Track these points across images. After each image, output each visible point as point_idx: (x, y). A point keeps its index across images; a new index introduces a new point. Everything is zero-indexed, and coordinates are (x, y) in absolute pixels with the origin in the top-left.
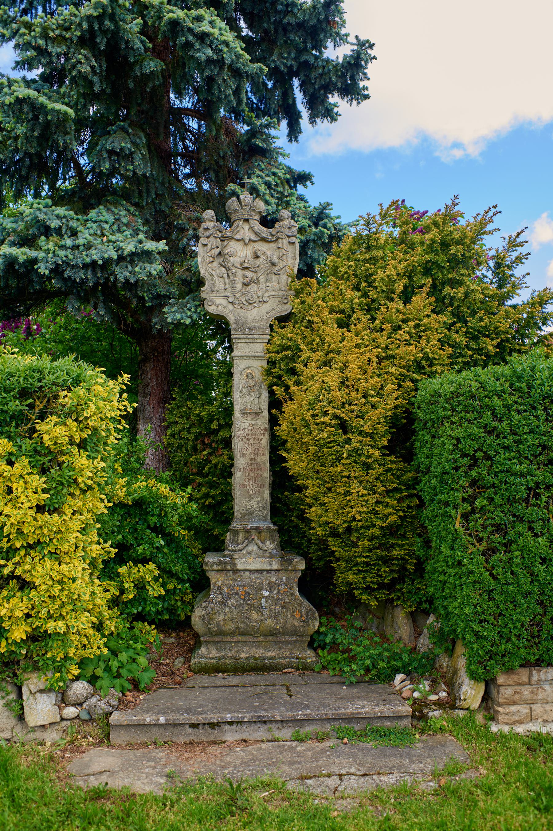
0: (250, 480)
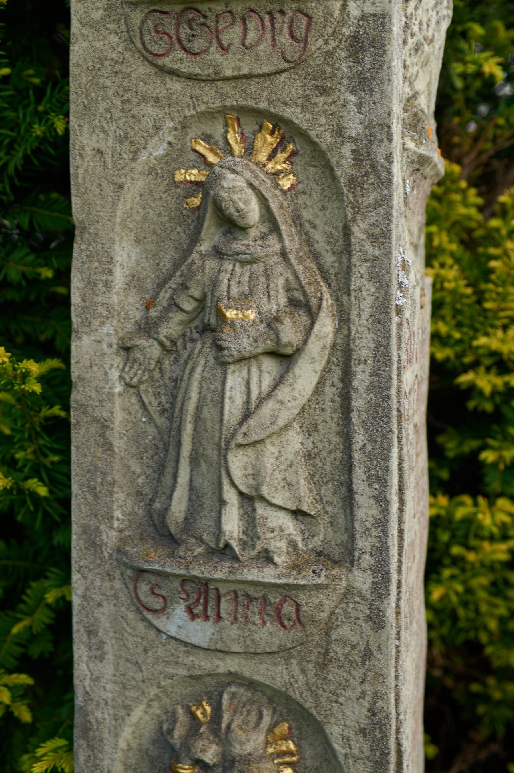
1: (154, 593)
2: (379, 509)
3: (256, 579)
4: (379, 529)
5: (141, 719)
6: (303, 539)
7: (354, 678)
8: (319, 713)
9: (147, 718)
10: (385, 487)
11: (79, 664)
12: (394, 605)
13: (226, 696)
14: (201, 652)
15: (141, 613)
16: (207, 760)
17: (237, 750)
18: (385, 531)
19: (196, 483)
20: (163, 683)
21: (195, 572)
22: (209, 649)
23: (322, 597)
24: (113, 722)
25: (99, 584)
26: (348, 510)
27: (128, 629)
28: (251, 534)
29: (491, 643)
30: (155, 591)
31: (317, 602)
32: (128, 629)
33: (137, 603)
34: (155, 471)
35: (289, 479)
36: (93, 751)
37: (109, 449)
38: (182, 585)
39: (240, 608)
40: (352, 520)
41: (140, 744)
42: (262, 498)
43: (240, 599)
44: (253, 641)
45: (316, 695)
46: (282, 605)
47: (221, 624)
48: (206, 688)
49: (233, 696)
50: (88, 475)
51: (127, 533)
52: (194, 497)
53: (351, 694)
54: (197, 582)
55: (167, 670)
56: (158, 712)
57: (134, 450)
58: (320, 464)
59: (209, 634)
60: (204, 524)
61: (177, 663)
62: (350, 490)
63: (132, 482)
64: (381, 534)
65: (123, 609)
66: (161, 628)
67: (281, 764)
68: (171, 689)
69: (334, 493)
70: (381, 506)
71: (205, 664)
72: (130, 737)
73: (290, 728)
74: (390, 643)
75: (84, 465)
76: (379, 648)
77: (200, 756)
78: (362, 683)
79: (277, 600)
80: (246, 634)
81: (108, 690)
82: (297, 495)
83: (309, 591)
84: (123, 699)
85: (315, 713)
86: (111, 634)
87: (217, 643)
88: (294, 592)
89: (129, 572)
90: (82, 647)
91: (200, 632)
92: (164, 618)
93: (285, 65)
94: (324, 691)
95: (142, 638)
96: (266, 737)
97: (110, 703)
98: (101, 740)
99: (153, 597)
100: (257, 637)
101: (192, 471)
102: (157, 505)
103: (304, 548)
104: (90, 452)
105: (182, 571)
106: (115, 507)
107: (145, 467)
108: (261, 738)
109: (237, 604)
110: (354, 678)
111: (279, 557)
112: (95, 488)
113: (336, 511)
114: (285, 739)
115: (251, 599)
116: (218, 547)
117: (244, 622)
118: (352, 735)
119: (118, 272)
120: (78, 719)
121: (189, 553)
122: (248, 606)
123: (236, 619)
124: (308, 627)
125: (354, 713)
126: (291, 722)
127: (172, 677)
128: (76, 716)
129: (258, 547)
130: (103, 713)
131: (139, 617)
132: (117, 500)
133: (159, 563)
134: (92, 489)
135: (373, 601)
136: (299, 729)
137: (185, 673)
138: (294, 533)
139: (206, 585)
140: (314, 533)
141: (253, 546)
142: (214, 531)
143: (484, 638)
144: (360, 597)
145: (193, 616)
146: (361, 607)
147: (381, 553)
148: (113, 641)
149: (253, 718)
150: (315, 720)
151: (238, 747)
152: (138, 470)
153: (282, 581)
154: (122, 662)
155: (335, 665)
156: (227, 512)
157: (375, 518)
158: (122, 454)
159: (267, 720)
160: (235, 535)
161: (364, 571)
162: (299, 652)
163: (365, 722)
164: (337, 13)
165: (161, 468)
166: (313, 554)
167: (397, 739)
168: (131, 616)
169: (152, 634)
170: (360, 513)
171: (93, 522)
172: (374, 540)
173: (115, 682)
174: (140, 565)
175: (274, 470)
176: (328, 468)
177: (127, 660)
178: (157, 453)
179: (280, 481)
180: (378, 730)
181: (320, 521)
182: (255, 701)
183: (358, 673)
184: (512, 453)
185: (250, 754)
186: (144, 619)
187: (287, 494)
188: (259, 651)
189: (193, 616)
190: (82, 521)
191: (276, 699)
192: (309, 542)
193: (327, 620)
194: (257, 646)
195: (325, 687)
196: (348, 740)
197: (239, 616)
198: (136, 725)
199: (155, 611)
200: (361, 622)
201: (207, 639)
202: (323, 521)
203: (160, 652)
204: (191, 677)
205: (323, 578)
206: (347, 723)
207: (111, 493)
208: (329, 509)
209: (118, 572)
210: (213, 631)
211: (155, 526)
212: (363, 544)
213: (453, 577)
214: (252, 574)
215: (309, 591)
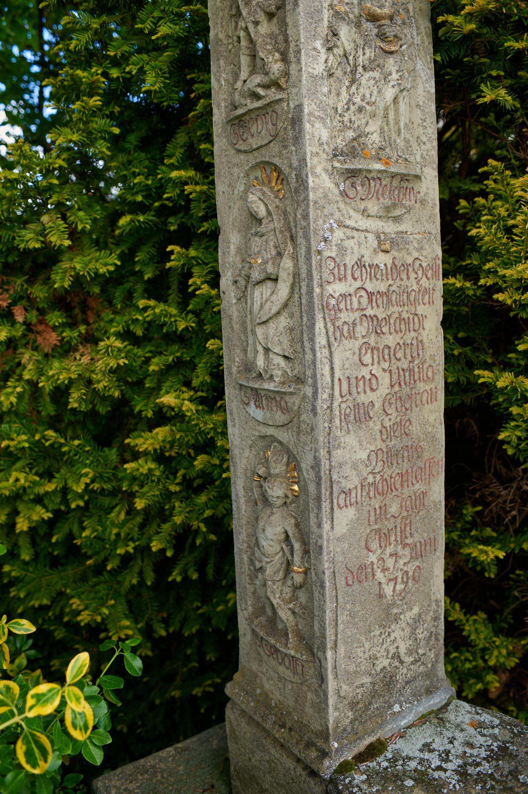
0: (384, 537)
93: (271, 138)
119: (232, 247)
149: (280, 458)
153: (276, 389)
164: (286, 108)
168: (241, 407)
183: (309, 437)
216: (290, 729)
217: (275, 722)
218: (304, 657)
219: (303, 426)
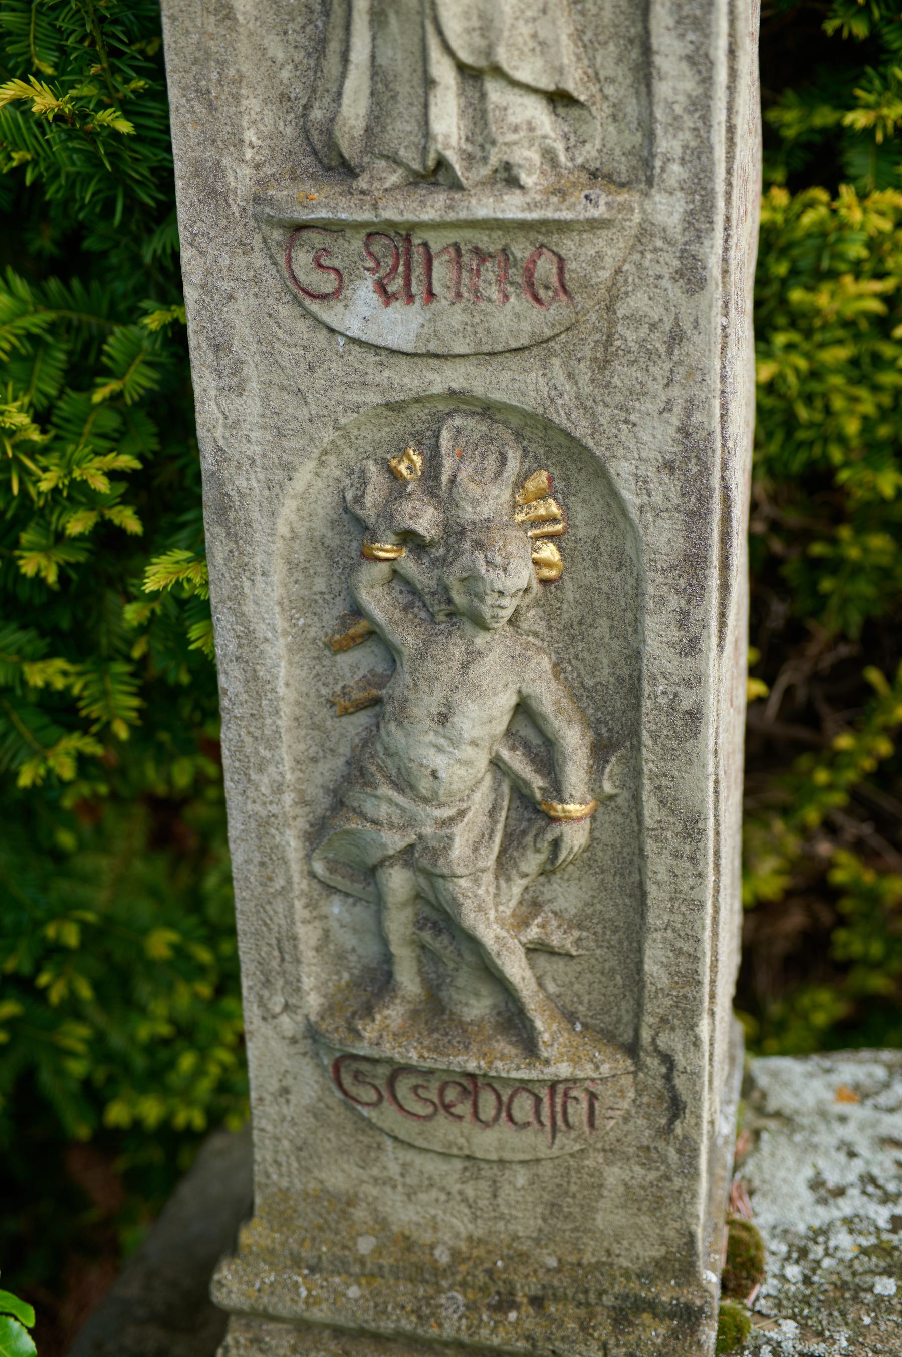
1: (320, 266)
2: (697, 78)
3: (491, 215)
4: (697, 115)
5: (310, 486)
6: (568, 149)
7: (655, 379)
8: (597, 444)
9: (320, 484)
10: (707, 36)
11: (203, 403)
12: (720, 251)
13: (445, 434)
14: (404, 361)
15: (300, 305)
16: (421, 531)
17: (467, 513)
18: (706, 119)
19: (381, 60)
20: (343, 421)
21: (389, 214)
22: (415, 355)
23: (602, 243)
24: (266, 493)
25: (227, 262)
26: (643, 89)
27: (280, 334)
28: (480, 139)
29: (847, 464)
30: (322, 262)
31: (593, 252)
32: (280, 334)
33: (292, 287)
34: (309, 55)
35: (542, 34)
36: (236, 542)
37: (227, 17)
38: (367, 246)
39: (465, 274)
40: (651, 104)
41: (310, 529)
42: (497, 71)
43: (465, 259)
44: (488, 331)
45: (593, 414)
46: (535, 262)
47: (434, 306)
48: (413, 426)
49: (458, 432)
50: (194, 68)
51: (268, 170)
52: (380, 86)
53: (650, 406)
54: (393, 234)
55: (348, 397)
56: (337, 473)
57: (270, 17)
58: (594, 10)
59: (414, 326)
60: (401, 132)
61: (364, 384)
62: (647, 50)
63: (271, 78)
64: (699, 124)
65: (270, 301)
66: (335, 325)
67: (538, 537)
68: (356, 432)
69: (619, 60)
70: (699, 72)
71: (410, 380)
72: (293, 517)
73: (550, 479)
74: (713, 313)
75: (187, 51)
76: (696, 324)
77: (410, 524)
78: (667, 385)
79: (527, 254)
80: (476, 320)
81: (255, 442)
82: (557, 63)
83: (580, 232)
84: (280, 452)
85: (591, 443)
86: (253, 347)
87: (428, 341)
88: (555, 237)
89: (277, 235)
90: (207, 373)
91: (401, 325)
92: (339, 307)
94: (606, 405)
95: (305, 348)
96: (513, 496)
97: (258, 462)
98: (248, 524)
99: (320, 271)
100: (494, 324)
101: (374, 38)
102: (317, 114)
103: (570, 165)
104: (195, 26)
105: (366, 215)
106: (245, 124)
107: (291, 49)
108: (506, 496)
109: (460, 268)
110: (655, 379)
111: (529, 174)
112: (209, 92)
113: (622, 92)
114: (542, 496)
115: (481, 255)
116: (425, 167)
117: (472, 298)
118: (651, 473)
120: (208, 493)
121: (376, 184)
122: (478, 271)
123: (459, 295)
124: (578, 298)
125: (654, 437)
126: (552, 469)
127: (357, 409)
128: (206, 488)
129: (494, 161)
130: (248, 480)
131: (298, 311)
132: (248, 110)
133: (327, 205)
134: (203, 94)
135: (686, 243)
136: (566, 479)
137: (378, 399)
138: (553, 135)
139: (408, 239)
140: (585, 137)
141: (485, 160)
142: (416, 140)
143: (837, 455)
144: (665, 239)
145: (388, 298)
146: (666, 257)
147: (699, 158)
148: (257, 359)
149: (491, 463)
150: (592, 455)
151: (470, 510)
152: (280, 56)
153: (535, 215)
154: (274, 392)
155: (624, 360)
156: (439, 101)
157: (689, 96)
158: (250, 25)
159: (513, 466)
160: (454, 141)
161: (671, 193)
162: (565, 344)
163: (672, 450)
165: (320, 46)
166: (584, 176)
167: (723, 478)
168: (285, 311)
169: (322, 336)
170: (663, 89)
171: (210, 153)
172: (687, 136)
173: (265, 428)
174: (296, 215)
175: (517, 18)
176: (608, 15)
177: (283, 388)
178: (310, 21)
179: (527, 38)
180: (694, 461)
181: (594, 112)
182: (492, 439)
183: (660, 370)
184: (901, 111)
185: (488, 520)
186: (307, 314)
187: (539, 63)
188: (499, 348)
189: (388, 298)
190: (191, 154)
191: (527, 432)
192: (577, 153)
193: (610, 284)
194: (495, 340)
195: (608, 399)
196: (646, 482)
197: (463, 290)
198: (303, 497)
199: (324, 297)
200: (666, 283)
201: (413, 336)
202: (601, 112)
203: (337, 368)
204: (388, 405)
205: (602, 208)
206: (644, 455)
207: (237, 98)
208: (610, 90)
209: (258, 237)
210: (421, 321)
211: (315, 153)
212: (668, 144)
213: (790, 347)
214: (484, 206)
215: (580, 232)
216: (537, 1302)
217: (471, 1307)
218: (605, 1069)
219: (629, 335)
